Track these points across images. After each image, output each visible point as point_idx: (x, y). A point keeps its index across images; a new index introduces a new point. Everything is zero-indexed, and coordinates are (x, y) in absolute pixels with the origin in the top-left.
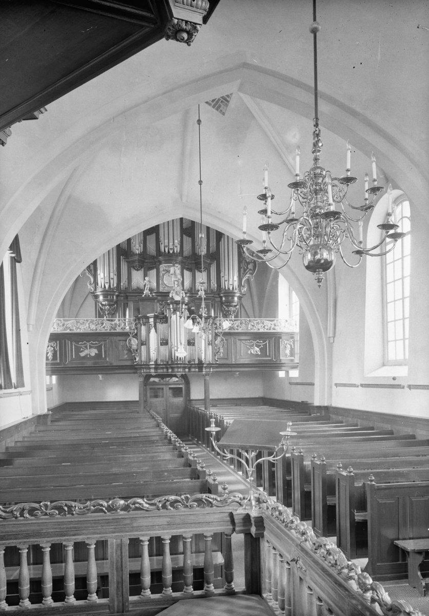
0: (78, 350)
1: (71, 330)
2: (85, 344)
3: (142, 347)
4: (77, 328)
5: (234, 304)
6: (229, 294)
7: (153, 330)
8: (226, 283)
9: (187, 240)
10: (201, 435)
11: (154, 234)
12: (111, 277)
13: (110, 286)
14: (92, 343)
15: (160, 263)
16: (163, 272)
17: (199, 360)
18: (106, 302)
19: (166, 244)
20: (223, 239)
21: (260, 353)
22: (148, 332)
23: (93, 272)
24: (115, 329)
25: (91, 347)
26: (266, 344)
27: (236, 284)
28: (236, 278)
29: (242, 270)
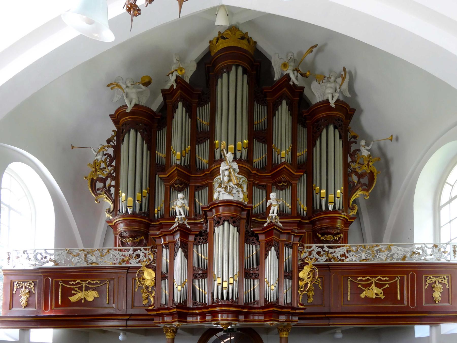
0: (67, 293)
2: (79, 283)
8: (323, 201)
14: (89, 283)
20: (318, 143)
21: (383, 297)
22: (173, 257)
23: (113, 195)
24: (128, 262)
25: (87, 289)
27: (339, 202)
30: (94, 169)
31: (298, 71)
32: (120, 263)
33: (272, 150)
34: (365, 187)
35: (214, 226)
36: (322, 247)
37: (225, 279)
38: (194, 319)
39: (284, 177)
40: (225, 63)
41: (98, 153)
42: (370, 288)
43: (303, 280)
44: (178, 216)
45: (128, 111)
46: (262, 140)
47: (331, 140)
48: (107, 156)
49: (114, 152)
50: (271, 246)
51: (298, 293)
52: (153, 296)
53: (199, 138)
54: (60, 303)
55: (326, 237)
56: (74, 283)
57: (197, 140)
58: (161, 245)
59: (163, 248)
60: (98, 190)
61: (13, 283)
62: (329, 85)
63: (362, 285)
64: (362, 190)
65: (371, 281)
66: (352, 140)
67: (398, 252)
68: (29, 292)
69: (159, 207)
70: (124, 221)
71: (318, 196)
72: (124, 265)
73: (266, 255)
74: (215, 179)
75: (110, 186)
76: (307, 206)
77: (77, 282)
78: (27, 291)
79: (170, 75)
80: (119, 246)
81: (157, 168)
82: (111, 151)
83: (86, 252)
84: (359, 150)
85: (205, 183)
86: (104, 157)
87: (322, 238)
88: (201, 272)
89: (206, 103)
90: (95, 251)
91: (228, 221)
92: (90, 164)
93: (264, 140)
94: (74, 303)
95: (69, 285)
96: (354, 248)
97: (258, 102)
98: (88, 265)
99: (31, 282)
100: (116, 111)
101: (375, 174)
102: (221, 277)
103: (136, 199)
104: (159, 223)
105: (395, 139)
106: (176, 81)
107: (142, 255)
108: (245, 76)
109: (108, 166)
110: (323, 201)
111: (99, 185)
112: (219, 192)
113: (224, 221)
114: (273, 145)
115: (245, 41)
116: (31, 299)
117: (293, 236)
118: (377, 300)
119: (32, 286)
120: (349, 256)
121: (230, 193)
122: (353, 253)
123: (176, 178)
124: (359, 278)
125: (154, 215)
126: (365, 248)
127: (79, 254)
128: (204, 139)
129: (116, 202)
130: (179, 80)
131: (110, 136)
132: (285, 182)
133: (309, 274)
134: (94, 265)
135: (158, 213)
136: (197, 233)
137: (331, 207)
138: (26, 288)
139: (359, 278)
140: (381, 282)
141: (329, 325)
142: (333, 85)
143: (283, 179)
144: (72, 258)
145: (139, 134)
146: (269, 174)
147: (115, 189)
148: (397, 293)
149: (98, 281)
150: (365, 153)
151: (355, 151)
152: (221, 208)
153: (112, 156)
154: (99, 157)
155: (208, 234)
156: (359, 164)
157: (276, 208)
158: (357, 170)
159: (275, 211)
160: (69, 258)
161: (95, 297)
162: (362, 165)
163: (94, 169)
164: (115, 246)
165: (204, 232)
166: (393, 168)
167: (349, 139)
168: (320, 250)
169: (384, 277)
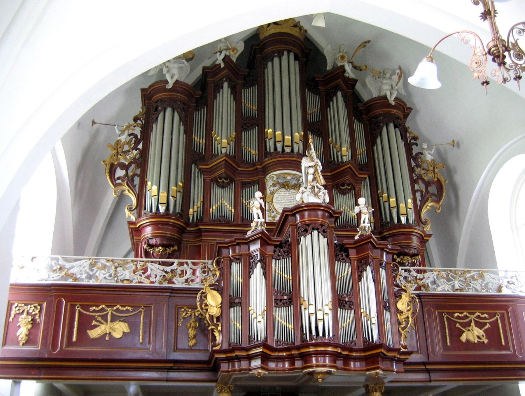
0: (86, 324)
1: (75, 279)
2: (103, 310)
3: (232, 310)
4: (90, 277)
5: (412, 251)
7: (258, 271)
8: (394, 211)
13: (167, 209)
14: (118, 310)
15: (265, 171)
16: (272, 189)
17: (365, 341)
18: (158, 239)
19: (279, 137)
20: (379, 141)
22: (247, 274)
23: (137, 188)
24: (170, 282)
26: (497, 318)
29: (418, 195)
30: (114, 152)
31: (352, 63)
32: (160, 283)
33: (330, 146)
34: (434, 198)
35: (300, 236)
36: (409, 271)
37: (319, 307)
38: (280, 365)
39: (348, 178)
40: (277, 48)
41: (123, 132)
42: (470, 328)
43: (402, 312)
44: (256, 220)
45: (170, 86)
46: (316, 132)
47: (391, 135)
48: (132, 137)
49: (141, 132)
50: (367, 264)
51: (399, 332)
52: (219, 331)
53: (245, 124)
54: (74, 339)
55: (402, 259)
56: (97, 309)
57: (243, 127)
58: (229, 257)
59: (231, 261)
60: (119, 178)
61: (12, 304)
62: (385, 81)
63: (461, 324)
64: (432, 201)
65: (469, 319)
66: (413, 141)
67: (492, 280)
68: (32, 320)
69: (195, 207)
70: (152, 224)
71: (387, 205)
72: (166, 284)
73: (360, 278)
74: (268, 176)
75: (134, 175)
76: (374, 217)
77: (101, 307)
78: (30, 318)
79: (218, 54)
80: (141, 257)
81: (196, 158)
82: (138, 131)
83: (116, 264)
84: (421, 154)
85: (256, 178)
86: (129, 138)
88: (287, 297)
89: (253, 85)
90: (127, 263)
91: (318, 229)
92: (110, 145)
93: (319, 132)
94: (94, 339)
95: (88, 311)
96: (444, 274)
97: (309, 90)
98: (117, 282)
99: (36, 304)
100: (150, 87)
101: (443, 183)
102: (314, 304)
103: (171, 194)
104: (197, 228)
105: (455, 144)
106: (223, 60)
107: (189, 272)
108: (297, 62)
109: (133, 149)
110: (394, 211)
111: (120, 173)
112: (303, 193)
113: (313, 229)
114: (330, 139)
115: (297, 29)
116: (33, 331)
117: (385, 253)
118: (480, 345)
119: (37, 311)
120: (440, 284)
121: (316, 195)
122: (439, 281)
123: (223, 171)
124: (456, 315)
125: (189, 217)
126: (456, 274)
127: (105, 266)
128: (251, 126)
129: (141, 197)
130: (226, 59)
131: (137, 113)
132: (348, 185)
133: (408, 305)
134: (126, 283)
135: (193, 215)
136: (278, 243)
137: (403, 220)
138: (28, 314)
139: (456, 315)
140: (480, 321)
141: (430, 381)
142: (389, 81)
143: (347, 182)
144: (97, 271)
145: (176, 114)
146: (329, 174)
147: (140, 179)
148: (500, 336)
149: (129, 308)
150: (429, 157)
151: (417, 154)
152: (306, 213)
153: (139, 137)
154: (124, 138)
155: (290, 245)
156: (424, 169)
157: (367, 216)
158: (423, 177)
159: (367, 221)
160: (92, 270)
161: (124, 333)
162: (428, 171)
163: (114, 152)
164: (136, 256)
165: (285, 243)
166: (457, 178)
167: (409, 140)
168: (406, 274)
169: (483, 314)
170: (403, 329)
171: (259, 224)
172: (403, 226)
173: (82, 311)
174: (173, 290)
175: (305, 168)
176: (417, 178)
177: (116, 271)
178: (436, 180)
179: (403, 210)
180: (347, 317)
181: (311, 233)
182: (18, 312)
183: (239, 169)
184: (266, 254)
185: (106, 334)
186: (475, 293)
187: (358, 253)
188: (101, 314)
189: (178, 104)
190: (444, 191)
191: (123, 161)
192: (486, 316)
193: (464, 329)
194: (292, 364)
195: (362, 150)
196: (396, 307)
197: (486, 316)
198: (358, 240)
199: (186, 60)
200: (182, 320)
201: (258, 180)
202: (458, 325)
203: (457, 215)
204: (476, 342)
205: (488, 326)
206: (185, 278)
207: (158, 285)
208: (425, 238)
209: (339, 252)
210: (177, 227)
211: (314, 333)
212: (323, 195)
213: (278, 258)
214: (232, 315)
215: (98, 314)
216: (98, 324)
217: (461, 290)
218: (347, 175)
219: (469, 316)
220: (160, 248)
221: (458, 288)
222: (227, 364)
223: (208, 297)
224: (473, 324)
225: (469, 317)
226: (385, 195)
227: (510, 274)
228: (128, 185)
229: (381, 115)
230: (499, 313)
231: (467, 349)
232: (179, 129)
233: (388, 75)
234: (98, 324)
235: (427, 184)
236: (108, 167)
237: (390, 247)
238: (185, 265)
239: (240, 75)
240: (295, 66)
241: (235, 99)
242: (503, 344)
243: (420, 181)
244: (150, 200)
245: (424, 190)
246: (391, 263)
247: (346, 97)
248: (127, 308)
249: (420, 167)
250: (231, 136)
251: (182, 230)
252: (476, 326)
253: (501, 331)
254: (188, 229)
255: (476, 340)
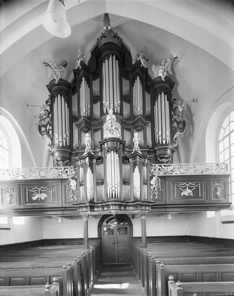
2: (36, 189)
4: (30, 176)
5: (167, 156)
6: (164, 147)
8: (160, 138)
9: (126, 106)
10: (21, 271)
11: (99, 102)
12: (64, 137)
13: (63, 143)
14: (42, 189)
17: (134, 198)
20: (156, 103)
21: (192, 195)
22: (85, 173)
23: (51, 136)
27: (168, 139)
28: (168, 133)
30: (40, 119)
33: (133, 107)
34: (181, 130)
36: (161, 166)
37: (113, 185)
39: (140, 123)
41: (42, 109)
42: (186, 190)
46: (127, 101)
47: (162, 99)
48: (46, 111)
49: (50, 109)
52: (76, 196)
53: (94, 100)
54: (27, 201)
56: (34, 189)
65: (186, 186)
66: (174, 101)
67: (199, 168)
69: (76, 142)
71: (157, 135)
72: (60, 177)
73: (134, 171)
75: (49, 130)
79: (78, 60)
82: (48, 108)
84: (177, 107)
85: (99, 127)
86: (45, 112)
87: (160, 160)
88: (100, 181)
89: (97, 78)
91: (113, 150)
93: (128, 101)
95: (31, 190)
101: (186, 122)
106: (81, 64)
108: (117, 61)
110: (160, 138)
114: (133, 104)
115: (116, 39)
117: (146, 159)
118: (189, 197)
123: (84, 125)
124: (180, 184)
126: (182, 166)
129: (52, 139)
130: (82, 63)
131: (47, 99)
132: (140, 127)
133: (156, 182)
134: (44, 178)
136: (98, 158)
137: (164, 142)
139: (180, 184)
141: (166, 212)
143: (139, 125)
145: (62, 97)
149: (46, 188)
151: (175, 108)
153: (49, 111)
155: (103, 158)
156: (177, 116)
159: (137, 145)
162: (179, 116)
167: (172, 101)
168: (160, 167)
170: (152, 192)
171: (88, 149)
172: (164, 145)
173: (29, 190)
174: (62, 179)
175: (108, 120)
176: (174, 121)
177: (39, 173)
178: (183, 121)
179: (164, 137)
180: (126, 188)
181: (111, 152)
182: (5, 192)
183: (92, 123)
184: (93, 163)
185: (39, 198)
186: (190, 174)
187: (133, 160)
188: (36, 191)
189: (63, 92)
190: (186, 126)
191: (44, 123)
192: (194, 184)
193: (183, 190)
194: (103, 208)
195: (148, 109)
196: (150, 183)
197: (194, 184)
198: (133, 154)
199: (63, 66)
200: (67, 191)
201: (100, 128)
202: (181, 189)
203: (193, 137)
204: (188, 195)
205: (194, 188)
206: (67, 174)
207: (57, 178)
208: (174, 150)
209: (124, 160)
210: (69, 152)
211: (111, 196)
212: (116, 133)
213: (98, 164)
214: (81, 190)
215: (35, 191)
216: (35, 194)
217: (184, 173)
218: (139, 122)
219: (186, 184)
220: (61, 161)
221: (182, 172)
222: (80, 209)
223: (71, 183)
224: (187, 188)
225: (186, 185)
226: (157, 130)
227: (209, 165)
228: (47, 134)
229: (158, 88)
230: (200, 183)
231: (189, 198)
232: (65, 105)
233: (163, 63)
234: (35, 194)
235: (178, 123)
236: (38, 127)
237: (149, 156)
238: (67, 169)
239: (91, 72)
240: (116, 63)
241: (89, 87)
242: (200, 196)
243: (175, 122)
244: (56, 142)
245: (176, 127)
246: (149, 164)
247: (142, 79)
248: (45, 188)
249: (176, 115)
250: (87, 107)
251: (70, 154)
252: (189, 189)
253: (200, 191)
254: (72, 152)
255: (188, 195)
